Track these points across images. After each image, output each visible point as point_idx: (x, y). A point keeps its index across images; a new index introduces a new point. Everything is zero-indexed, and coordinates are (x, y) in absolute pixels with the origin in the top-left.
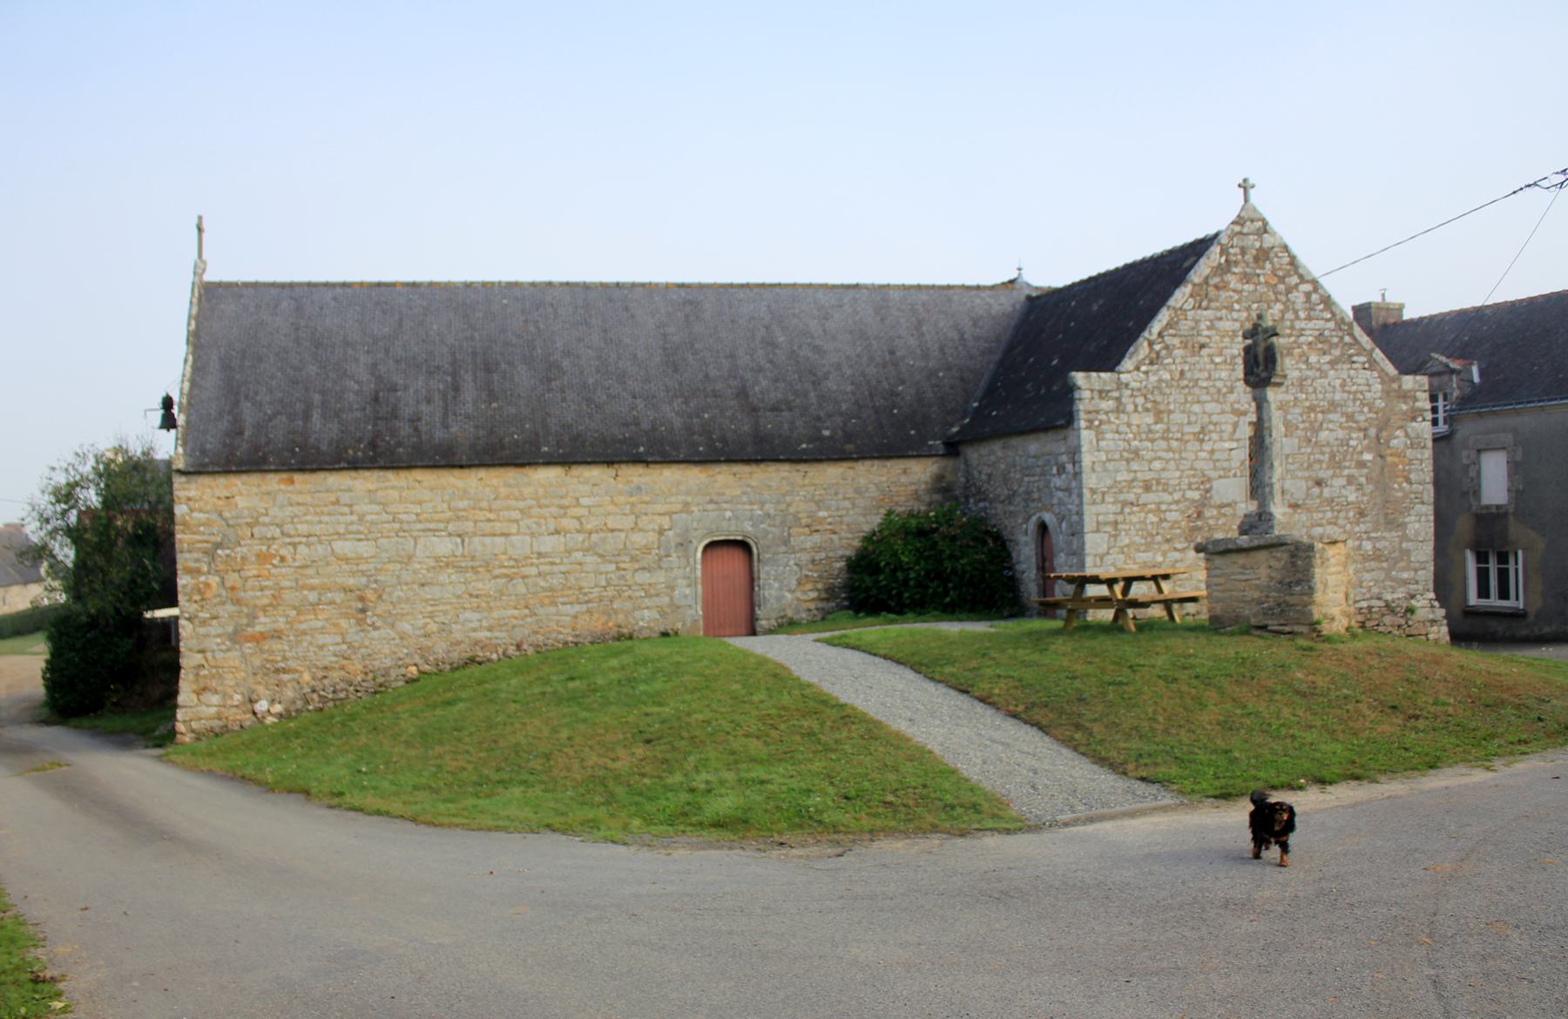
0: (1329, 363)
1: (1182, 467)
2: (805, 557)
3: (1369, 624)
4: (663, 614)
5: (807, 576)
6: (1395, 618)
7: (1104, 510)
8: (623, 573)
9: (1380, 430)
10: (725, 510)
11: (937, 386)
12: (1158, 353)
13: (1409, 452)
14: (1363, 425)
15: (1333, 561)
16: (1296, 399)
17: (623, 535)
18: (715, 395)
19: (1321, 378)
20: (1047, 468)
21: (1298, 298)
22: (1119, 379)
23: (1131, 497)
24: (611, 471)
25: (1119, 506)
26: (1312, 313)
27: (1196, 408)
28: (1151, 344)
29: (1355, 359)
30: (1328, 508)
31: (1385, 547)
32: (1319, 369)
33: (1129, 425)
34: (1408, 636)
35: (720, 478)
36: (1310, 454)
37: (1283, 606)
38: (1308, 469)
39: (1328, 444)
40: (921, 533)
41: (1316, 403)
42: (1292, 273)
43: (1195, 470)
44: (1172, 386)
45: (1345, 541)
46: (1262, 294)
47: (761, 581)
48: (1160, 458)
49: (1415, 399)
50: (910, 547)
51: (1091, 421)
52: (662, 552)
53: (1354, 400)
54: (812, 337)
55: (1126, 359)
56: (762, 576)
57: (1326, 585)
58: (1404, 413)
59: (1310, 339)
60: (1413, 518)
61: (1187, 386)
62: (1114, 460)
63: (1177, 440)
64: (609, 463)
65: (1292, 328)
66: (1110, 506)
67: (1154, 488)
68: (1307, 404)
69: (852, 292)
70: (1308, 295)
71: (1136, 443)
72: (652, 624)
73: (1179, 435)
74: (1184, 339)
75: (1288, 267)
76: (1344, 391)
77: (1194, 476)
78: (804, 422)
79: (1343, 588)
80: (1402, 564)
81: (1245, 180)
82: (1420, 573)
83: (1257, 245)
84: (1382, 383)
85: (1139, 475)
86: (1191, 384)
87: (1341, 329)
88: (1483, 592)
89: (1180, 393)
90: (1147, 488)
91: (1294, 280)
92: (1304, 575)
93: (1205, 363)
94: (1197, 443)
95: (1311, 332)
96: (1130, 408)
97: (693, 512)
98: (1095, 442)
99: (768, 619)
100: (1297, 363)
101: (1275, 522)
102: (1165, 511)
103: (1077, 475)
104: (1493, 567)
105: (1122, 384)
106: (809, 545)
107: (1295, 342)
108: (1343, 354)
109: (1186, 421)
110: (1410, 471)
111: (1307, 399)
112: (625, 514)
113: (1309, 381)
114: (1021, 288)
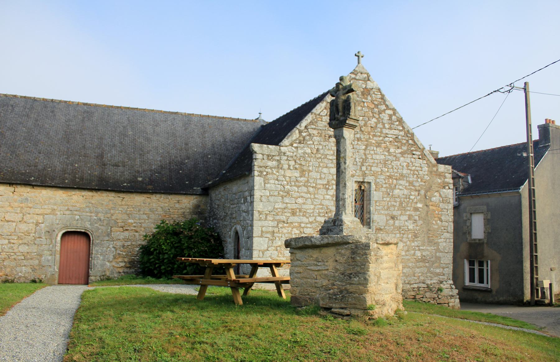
0: (400, 153)
1: (315, 203)
2: (119, 244)
3: (417, 297)
4: (34, 270)
5: (119, 254)
6: (432, 294)
7: (266, 224)
8: (12, 245)
9: (426, 191)
10: (76, 215)
11: (206, 162)
12: (304, 138)
13: (441, 205)
14: (418, 188)
15: (385, 258)
16: (382, 170)
17: (14, 224)
18: (85, 156)
19: (396, 161)
20: (239, 199)
21: (385, 117)
22: (280, 149)
23: (283, 218)
24: (11, 189)
25: (276, 222)
26: (392, 126)
27: (325, 170)
28: (300, 132)
29: (414, 152)
30: (398, 232)
31: (427, 255)
32: (395, 156)
33: (284, 176)
34: (438, 304)
35: (75, 197)
36: (388, 201)
37: (345, 292)
38: (387, 210)
39: (399, 196)
40: (175, 233)
41: (393, 174)
42: (382, 103)
43: (323, 205)
44: (312, 157)
45: (396, 244)
46: (365, 112)
47: (93, 255)
48: (302, 197)
49: (445, 177)
50: (168, 241)
51: (261, 172)
52: (37, 235)
53: (414, 174)
54: (147, 133)
55: (285, 139)
56: (94, 252)
57: (379, 277)
58: (439, 184)
59: (391, 139)
60: (442, 240)
61: (320, 158)
62: (275, 196)
63: (313, 187)
64: (11, 184)
65: (381, 132)
66: (270, 222)
67: (298, 214)
68: (388, 174)
69: (173, 116)
70: (390, 116)
71: (287, 187)
72: (27, 275)
73: (314, 185)
74: (320, 132)
75: (380, 100)
76: (408, 169)
77: (322, 208)
78: (129, 173)
79: (394, 280)
80: (436, 265)
81: (359, 52)
82: (445, 269)
83: (364, 86)
84: (429, 167)
85: (289, 205)
86: (323, 157)
87: (407, 136)
88: (472, 280)
89: (316, 161)
90: (294, 213)
91: (383, 107)
92: (362, 269)
93: (332, 146)
94: (325, 190)
95: (391, 136)
96: (286, 166)
97: (57, 214)
98: (263, 185)
99: (95, 276)
100: (383, 152)
101: (344, 227)
102: (303, 228)
103: (252, 202)
104: (476, 268)
105: (281, 152)
106: (121, 237)
107: (383, 140)
108: (408, 150)
109: (319, 177)
110: (441, 215)
111: (388, 171)
112: (17, 213)
113: (390, 162)
114: (260, 122)
